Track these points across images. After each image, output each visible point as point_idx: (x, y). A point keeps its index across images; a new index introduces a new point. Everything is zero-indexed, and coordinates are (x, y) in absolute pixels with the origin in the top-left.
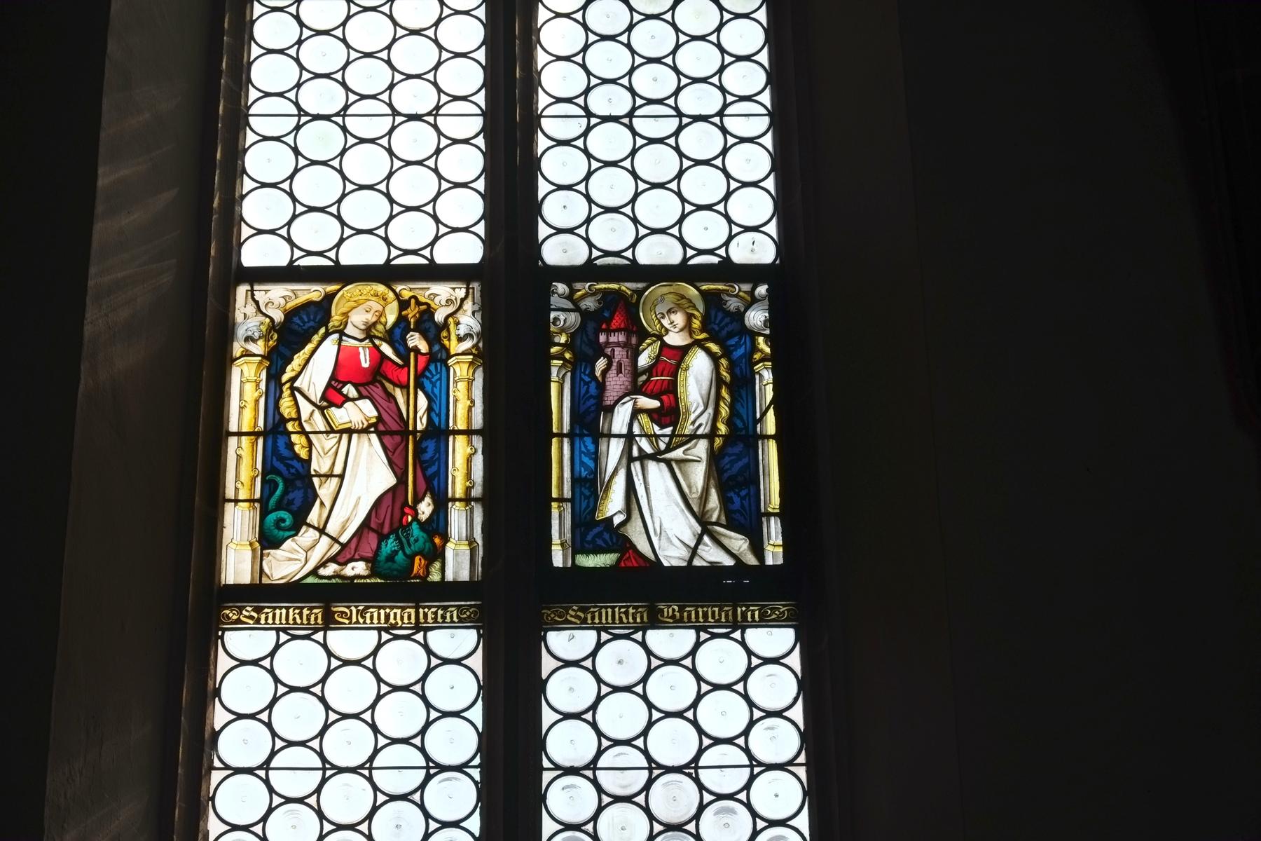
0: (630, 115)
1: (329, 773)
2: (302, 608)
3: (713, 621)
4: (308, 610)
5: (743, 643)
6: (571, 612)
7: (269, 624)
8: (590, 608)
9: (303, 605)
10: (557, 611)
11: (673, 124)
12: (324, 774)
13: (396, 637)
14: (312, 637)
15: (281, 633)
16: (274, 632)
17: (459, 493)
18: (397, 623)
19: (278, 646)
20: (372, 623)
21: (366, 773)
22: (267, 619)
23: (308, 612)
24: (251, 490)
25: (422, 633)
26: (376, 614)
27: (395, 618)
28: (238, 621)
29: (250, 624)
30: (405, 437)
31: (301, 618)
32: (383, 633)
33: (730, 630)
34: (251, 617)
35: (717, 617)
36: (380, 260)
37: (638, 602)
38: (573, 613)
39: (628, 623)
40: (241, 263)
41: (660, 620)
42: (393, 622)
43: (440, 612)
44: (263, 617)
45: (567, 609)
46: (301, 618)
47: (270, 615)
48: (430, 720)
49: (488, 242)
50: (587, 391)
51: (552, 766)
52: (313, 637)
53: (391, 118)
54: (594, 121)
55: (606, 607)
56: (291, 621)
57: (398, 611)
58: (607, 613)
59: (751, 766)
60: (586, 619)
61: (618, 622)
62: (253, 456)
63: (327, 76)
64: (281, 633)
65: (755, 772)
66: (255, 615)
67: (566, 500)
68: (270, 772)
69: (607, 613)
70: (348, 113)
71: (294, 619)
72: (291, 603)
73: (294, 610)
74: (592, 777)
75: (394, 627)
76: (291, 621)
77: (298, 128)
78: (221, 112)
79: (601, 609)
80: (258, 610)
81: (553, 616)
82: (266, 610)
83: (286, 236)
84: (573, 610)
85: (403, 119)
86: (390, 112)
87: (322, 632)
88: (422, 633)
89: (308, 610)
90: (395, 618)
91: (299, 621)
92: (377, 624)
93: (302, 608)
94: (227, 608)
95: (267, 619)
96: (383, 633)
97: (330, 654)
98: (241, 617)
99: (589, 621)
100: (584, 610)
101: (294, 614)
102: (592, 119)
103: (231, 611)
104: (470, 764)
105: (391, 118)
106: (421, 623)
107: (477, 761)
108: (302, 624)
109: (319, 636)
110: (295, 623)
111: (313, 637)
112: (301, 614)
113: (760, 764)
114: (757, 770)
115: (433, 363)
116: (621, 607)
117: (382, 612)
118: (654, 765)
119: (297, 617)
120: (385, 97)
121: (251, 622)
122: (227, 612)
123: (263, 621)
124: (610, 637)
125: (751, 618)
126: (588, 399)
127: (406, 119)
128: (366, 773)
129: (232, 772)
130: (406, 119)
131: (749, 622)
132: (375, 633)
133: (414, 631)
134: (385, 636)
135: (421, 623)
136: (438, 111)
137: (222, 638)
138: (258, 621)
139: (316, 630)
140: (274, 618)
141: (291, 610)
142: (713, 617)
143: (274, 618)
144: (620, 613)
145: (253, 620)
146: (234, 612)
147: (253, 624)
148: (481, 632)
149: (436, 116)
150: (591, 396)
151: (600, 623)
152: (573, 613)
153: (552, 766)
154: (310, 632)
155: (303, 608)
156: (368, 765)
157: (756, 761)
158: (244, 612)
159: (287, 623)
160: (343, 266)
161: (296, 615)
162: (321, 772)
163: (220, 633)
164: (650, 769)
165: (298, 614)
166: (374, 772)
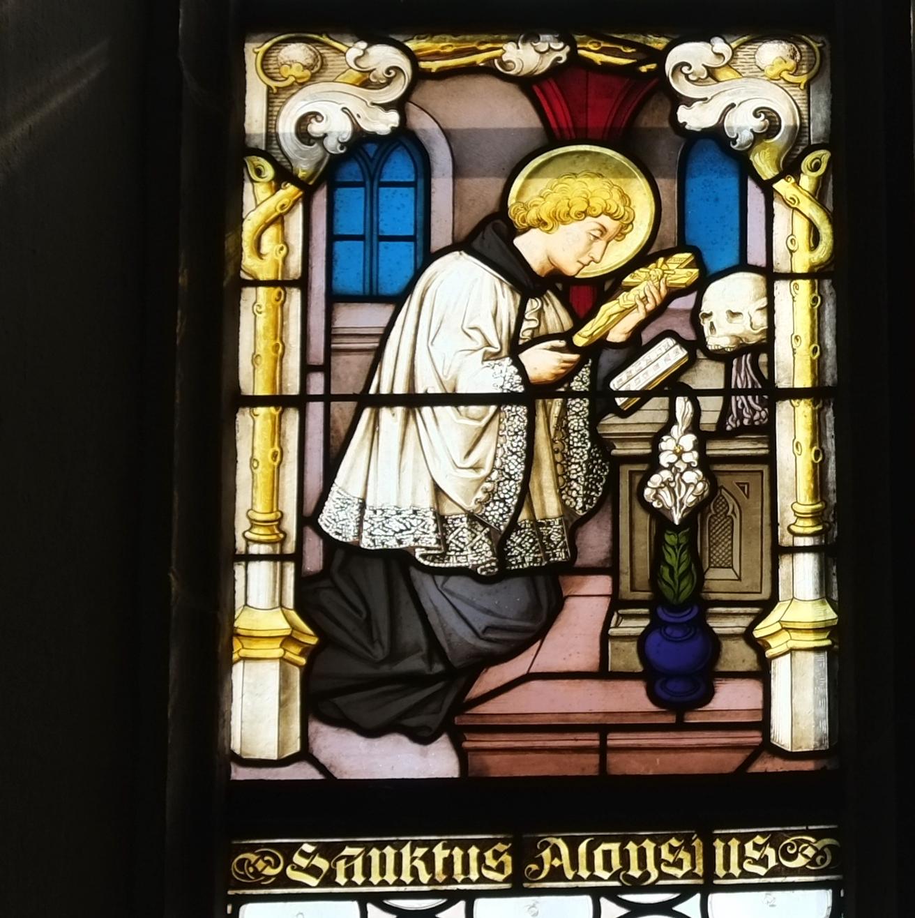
2: (431, 845)
3: (606, 875)
4: (445, 847)
6: (298, 859)
7: (355, 885)
8: (342, 846)
15: (370, 907)
18: (647, 875)
20: (351, 883)
22: (349, 872)
23: (447, 853)
24: (273, 496)
28: (283, 880)
30: (599, 388)
31: (431, 868)
34: (313, 871)
38: (303, 862)
39: (577, 878)
41: (787, 868)
43: (458, 853)
44: (341, 866)
45: (289, 851)
46: (431, 868)
47: (358, 864)
55: (381, 846)
56: (406, 877)
58: (383, 858)
60: (332, 872)
61: (460, 878)
62: (274, 378)
64: (370, 907)
66: (322, 864)
69: (383, 858)
71: (414, 872)
73: (412, 851)
75: (638, 886)
76: (406, 877)
79: (367, 850)
82: (348, 851)
84: (304, 855)
87: (698, 897)
89: (445, 847)
91: (424, 877)
94: (252, 848)
95: (349, 872)
98: (289, 870)
99: (341, 879)
100: (330, 852)
101: (413, 859)
103: (262, 855)
106: (718, 878)
110: (416, 882)
112: (429, 859)
115: (577, 52)
116: (415, 845)
119: (421, 865)
121: (312, 881)
122: (252, 857)
123: (341, 879)
125: (444, 872)
131: (338, 885)
135: (718, 878)
138: (329, 879)
140: (367, 872)
141: (406, 851)
142: (607, 865)
143: (367, 872)
144: (413, 859)
145: (317, 877)
147: (318, 886)
148: (842, 894)
152: (303, 862)
158: (298, 859)
159: (399, 883)
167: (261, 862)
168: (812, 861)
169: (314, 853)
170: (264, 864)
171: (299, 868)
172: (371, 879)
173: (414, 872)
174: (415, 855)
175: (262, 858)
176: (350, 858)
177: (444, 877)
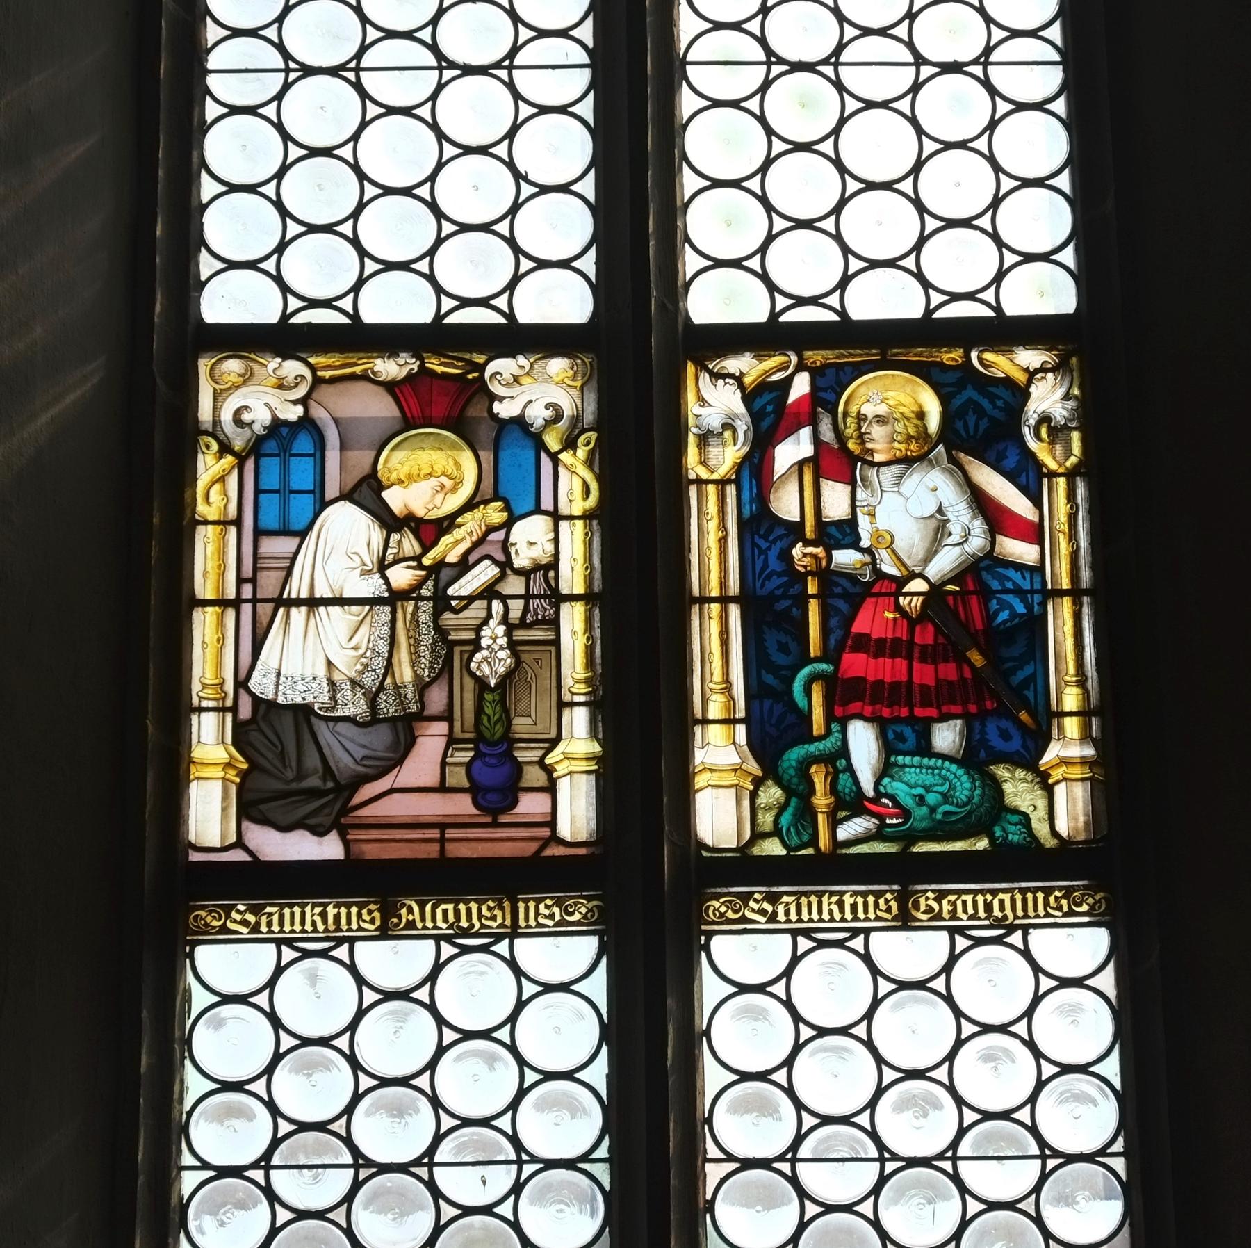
0: (984, 57)
1: (528, 1169)
3: (444, 926)
5: (1026, 953)
6: (234, 915)
8: (264, 906)
9: (844, 888)
10: (730, 902)
11: (906, 76)
12: (1044, 1166)
13: (466, 950)
14: (1006, 940)
15: (442, 943)
16: (788, 937)
17: (715, 711)
19: (795, 960)
21: (947, 1166)
22: (270, 924)
25: (346, 946)
26: (443, 914)
27: (1002, 908)
29: (549, 927)
31: (842, 911)
32: (284, 948)
33: (334, 943)
34: (245, 923)
35: (971, 911)
36: (759, 314)
37: (574, 892)
38: (756, 906)
39: (425, 928)
40: (849, 317)
42: (1000, 915)
44: (781, 909)
45: (228, 910)
46: (325, 921)
47: (275, 918)
48: (884, 1085)
49: (1084, 277)
50: (765, 565)
51: (722, 1156)
52: (494, 948)
53: (914, 68)
54: (926, 71)
55: (291, 906)
57: (1006, 897)
58: (292, 914)
59: (1043, 1158)
63: (253, 33)
64: (442, 943)
65: (887, 1171)
67: (740, 721)
68: (436, 1169)
69: (292, 914)
70: (992, 59)
71: (314, 923)
72: (796, 885)
74: (950, 1170)
75: (466, 933)
76: (308, 927)
77: (916, 88)
78: (649, 72)
79: (282, 909)
80: (773, 899)
81: (723, 909)
82: (785, 899)
83: (759, 271)
84: (239, 912)
85: (931, 70)
86: (911, 60)
88: (346, 946)
89: (334, 907)
90: (1002, 908)
91: (321, 927)
92: (267, 933)
93: (878, 895)
96: (284, 948)
97: (361, 981)
100: (256, 910)
101: (313, 915)
102: (922, 68)
103: (210, 912)
104: (1108, 1151)
105: (914, 68)
107: (1118, 1146)
108: (326, 930)
109: (502, 948)
111: (494, 948)
113: (1056, 1154)
114: (1051, 1163)
117: (980, 898)
118: (887, 1155)
119: (318, 919)
120: (901, 31)
121: (763, 919)
122: (203, 914)
124: (456, 951)
125: (334, 924)
126: (769, 577)
127: (938, 70)
128: (947, 1166)
129: (904, 1164)
130: (938, 70)
132: (787, 938)
133: (334, 943)
134: (447, 950)
135: (521, 928)
136: (987, 57)
137: (191, 956)
138: (256, 928)
139: (498, 938)
140: (281, 924)
141: (308, 909)
143: (281, 924)
144: (830, 904)
146: (213, 914)
147: (248, 933)
148: (605, 939)
149: (986, 65)
150: (773, 573)
151: (800, 921)
152: (756, 906)
153: (722, 1156)
154: (1002, 932)
155: (327, 904)
156: (949, 1154)
157: (1051, 1148)
158: (234, 915)
160: (768, 319)
161: (832, 907)
162: (352, 1171)
163: (188, 949)
164: (356, 1167)
165: (836, 903)
166: (960, 1164)
167: (209, 917)
168: (585, 917)
169: (763, 899)
170: (211, 919)
171: (753, 910)
172: (284, 929)
173: (314, 923)
174: (831, 900)
175: (210, 914)
176: (270, 915)
177: (334, 927)
